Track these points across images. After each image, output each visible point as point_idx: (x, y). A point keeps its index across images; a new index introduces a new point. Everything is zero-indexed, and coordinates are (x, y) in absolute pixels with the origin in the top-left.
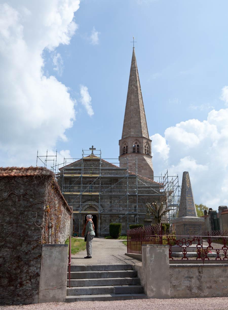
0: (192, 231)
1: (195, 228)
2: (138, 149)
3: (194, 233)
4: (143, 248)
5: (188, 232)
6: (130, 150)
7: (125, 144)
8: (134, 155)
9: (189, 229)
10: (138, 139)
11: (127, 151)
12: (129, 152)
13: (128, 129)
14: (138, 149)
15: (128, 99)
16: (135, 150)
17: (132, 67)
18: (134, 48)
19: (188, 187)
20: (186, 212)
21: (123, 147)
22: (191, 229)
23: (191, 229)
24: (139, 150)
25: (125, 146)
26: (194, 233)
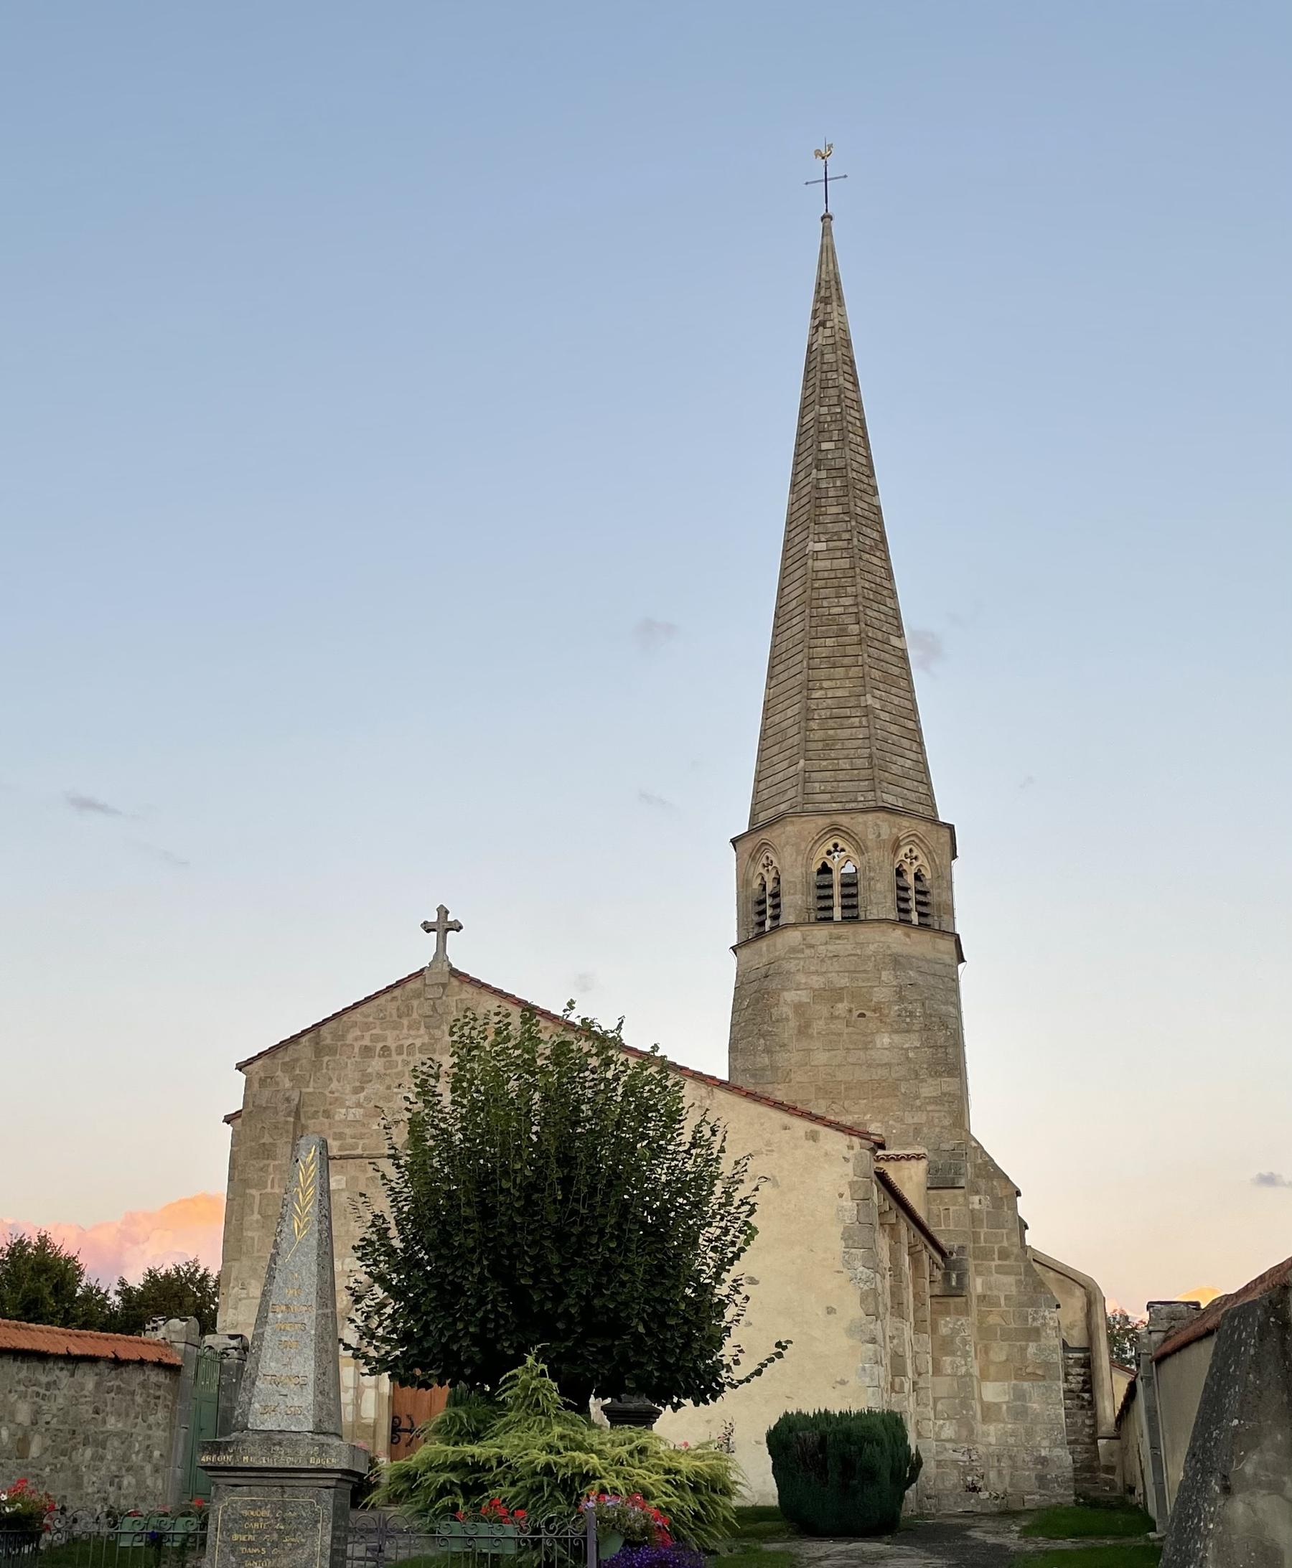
0: (260, 1533)
1: (284, 1512)
2: (852, 890)
3: (275, 1544)
4: (996, 1266)
5: (235, 1537)
6: (794, 902)
7: (764, 861)
8: (821, 933)
9: (245, 1519)
10: (844, 820)
11: (777, 900)
12: (787, 916)
13: (785, 764)
14: (852, 890)
15: (802, 475)
16: (831, 897)
17: (814, 347)
18: (826, 218)
19: (299, 1238)
20: (250, 1404)
21: (756, 884)
22: (256, 1519)
23: (256, 1519)
24: (855, 907)
25: (769, 878)
26: (275, 1544)
